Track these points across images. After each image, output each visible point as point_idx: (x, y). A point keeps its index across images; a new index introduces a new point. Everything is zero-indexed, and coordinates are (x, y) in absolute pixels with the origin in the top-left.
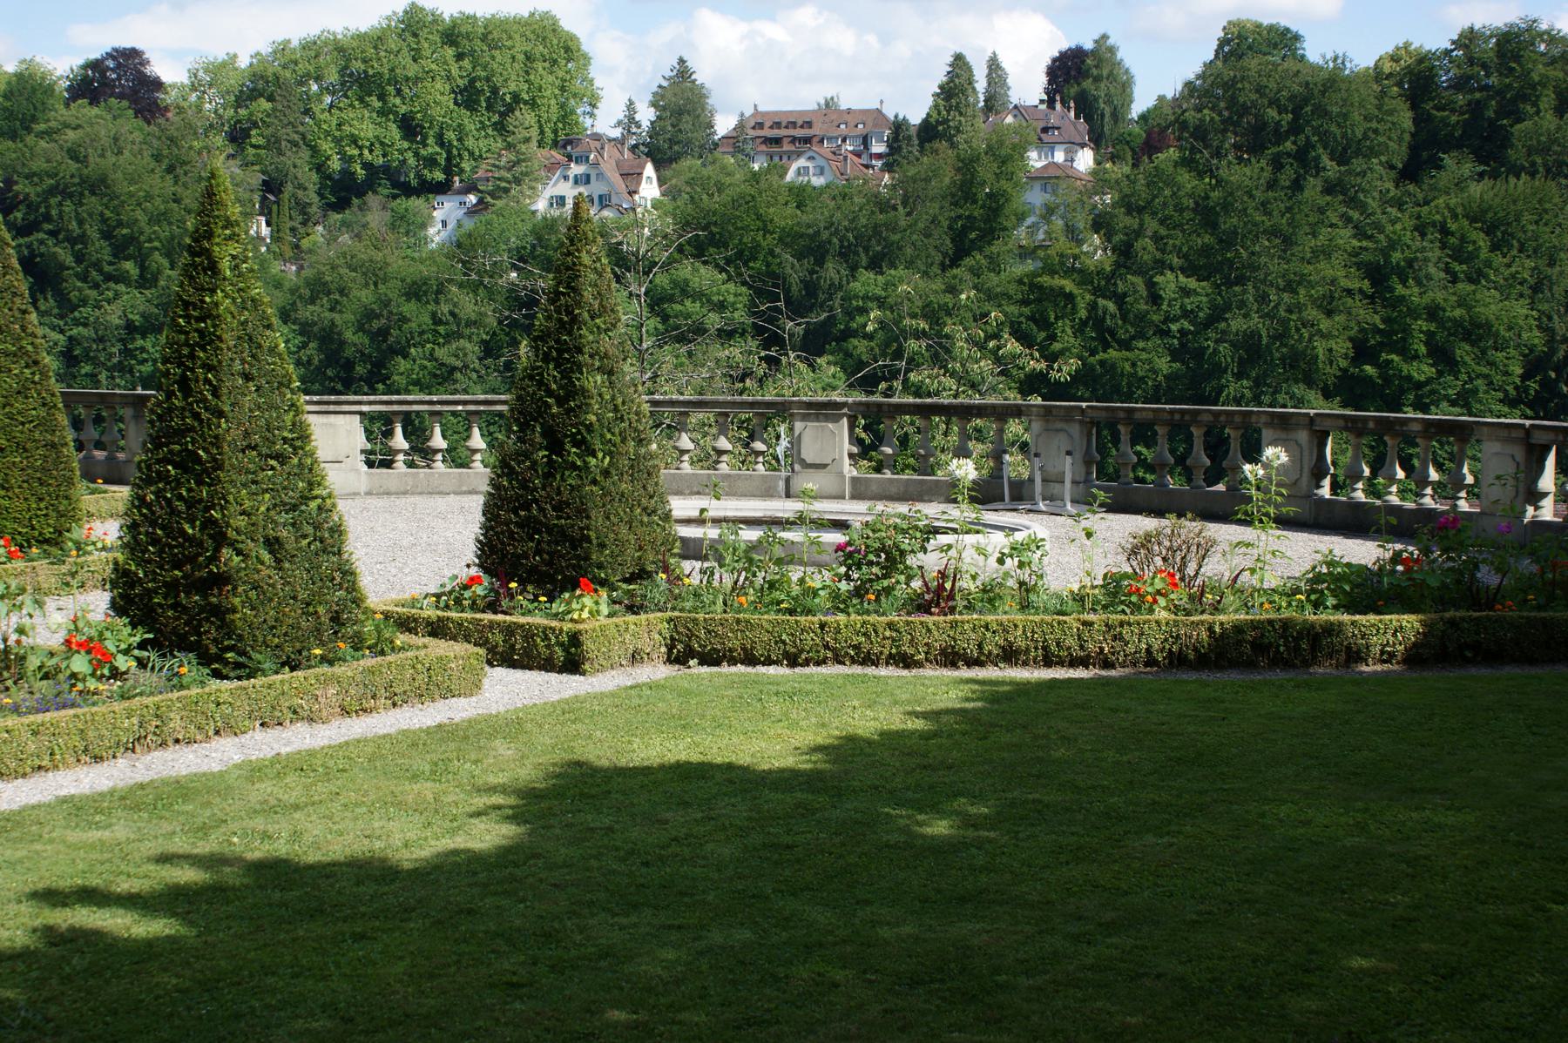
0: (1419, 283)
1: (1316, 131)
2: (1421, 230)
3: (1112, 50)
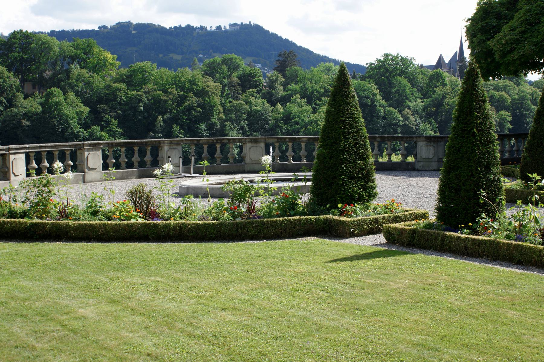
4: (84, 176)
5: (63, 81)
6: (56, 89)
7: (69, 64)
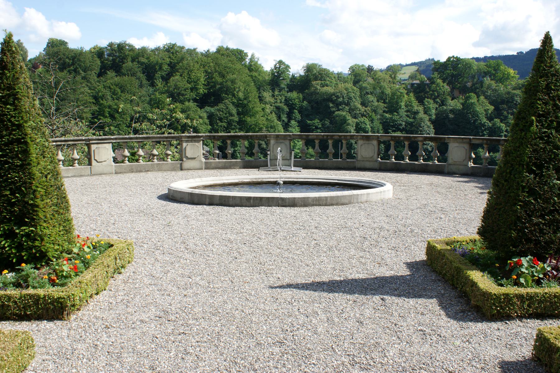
0: (106, 100)
1: (78, 65)
2: (104, 87)
3: (22, 44)
4: (181, 164)
5: (478, 88)
6: (472, 94)
7: (483, 77)
